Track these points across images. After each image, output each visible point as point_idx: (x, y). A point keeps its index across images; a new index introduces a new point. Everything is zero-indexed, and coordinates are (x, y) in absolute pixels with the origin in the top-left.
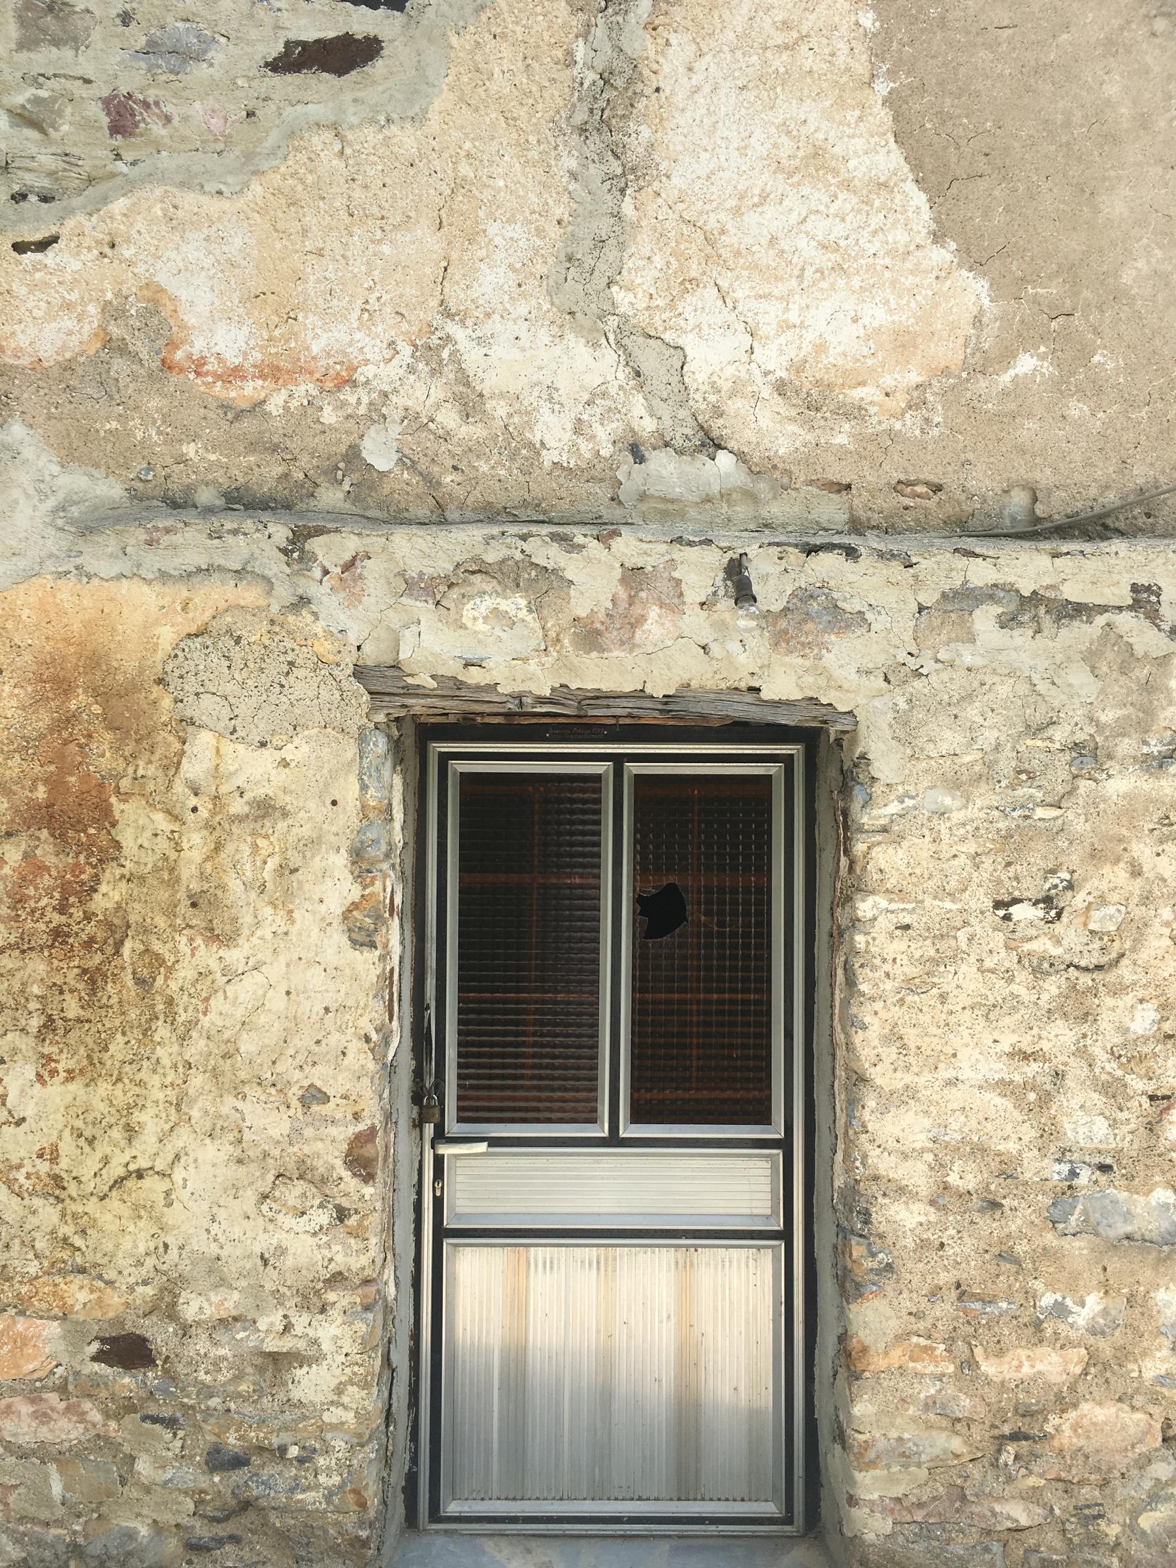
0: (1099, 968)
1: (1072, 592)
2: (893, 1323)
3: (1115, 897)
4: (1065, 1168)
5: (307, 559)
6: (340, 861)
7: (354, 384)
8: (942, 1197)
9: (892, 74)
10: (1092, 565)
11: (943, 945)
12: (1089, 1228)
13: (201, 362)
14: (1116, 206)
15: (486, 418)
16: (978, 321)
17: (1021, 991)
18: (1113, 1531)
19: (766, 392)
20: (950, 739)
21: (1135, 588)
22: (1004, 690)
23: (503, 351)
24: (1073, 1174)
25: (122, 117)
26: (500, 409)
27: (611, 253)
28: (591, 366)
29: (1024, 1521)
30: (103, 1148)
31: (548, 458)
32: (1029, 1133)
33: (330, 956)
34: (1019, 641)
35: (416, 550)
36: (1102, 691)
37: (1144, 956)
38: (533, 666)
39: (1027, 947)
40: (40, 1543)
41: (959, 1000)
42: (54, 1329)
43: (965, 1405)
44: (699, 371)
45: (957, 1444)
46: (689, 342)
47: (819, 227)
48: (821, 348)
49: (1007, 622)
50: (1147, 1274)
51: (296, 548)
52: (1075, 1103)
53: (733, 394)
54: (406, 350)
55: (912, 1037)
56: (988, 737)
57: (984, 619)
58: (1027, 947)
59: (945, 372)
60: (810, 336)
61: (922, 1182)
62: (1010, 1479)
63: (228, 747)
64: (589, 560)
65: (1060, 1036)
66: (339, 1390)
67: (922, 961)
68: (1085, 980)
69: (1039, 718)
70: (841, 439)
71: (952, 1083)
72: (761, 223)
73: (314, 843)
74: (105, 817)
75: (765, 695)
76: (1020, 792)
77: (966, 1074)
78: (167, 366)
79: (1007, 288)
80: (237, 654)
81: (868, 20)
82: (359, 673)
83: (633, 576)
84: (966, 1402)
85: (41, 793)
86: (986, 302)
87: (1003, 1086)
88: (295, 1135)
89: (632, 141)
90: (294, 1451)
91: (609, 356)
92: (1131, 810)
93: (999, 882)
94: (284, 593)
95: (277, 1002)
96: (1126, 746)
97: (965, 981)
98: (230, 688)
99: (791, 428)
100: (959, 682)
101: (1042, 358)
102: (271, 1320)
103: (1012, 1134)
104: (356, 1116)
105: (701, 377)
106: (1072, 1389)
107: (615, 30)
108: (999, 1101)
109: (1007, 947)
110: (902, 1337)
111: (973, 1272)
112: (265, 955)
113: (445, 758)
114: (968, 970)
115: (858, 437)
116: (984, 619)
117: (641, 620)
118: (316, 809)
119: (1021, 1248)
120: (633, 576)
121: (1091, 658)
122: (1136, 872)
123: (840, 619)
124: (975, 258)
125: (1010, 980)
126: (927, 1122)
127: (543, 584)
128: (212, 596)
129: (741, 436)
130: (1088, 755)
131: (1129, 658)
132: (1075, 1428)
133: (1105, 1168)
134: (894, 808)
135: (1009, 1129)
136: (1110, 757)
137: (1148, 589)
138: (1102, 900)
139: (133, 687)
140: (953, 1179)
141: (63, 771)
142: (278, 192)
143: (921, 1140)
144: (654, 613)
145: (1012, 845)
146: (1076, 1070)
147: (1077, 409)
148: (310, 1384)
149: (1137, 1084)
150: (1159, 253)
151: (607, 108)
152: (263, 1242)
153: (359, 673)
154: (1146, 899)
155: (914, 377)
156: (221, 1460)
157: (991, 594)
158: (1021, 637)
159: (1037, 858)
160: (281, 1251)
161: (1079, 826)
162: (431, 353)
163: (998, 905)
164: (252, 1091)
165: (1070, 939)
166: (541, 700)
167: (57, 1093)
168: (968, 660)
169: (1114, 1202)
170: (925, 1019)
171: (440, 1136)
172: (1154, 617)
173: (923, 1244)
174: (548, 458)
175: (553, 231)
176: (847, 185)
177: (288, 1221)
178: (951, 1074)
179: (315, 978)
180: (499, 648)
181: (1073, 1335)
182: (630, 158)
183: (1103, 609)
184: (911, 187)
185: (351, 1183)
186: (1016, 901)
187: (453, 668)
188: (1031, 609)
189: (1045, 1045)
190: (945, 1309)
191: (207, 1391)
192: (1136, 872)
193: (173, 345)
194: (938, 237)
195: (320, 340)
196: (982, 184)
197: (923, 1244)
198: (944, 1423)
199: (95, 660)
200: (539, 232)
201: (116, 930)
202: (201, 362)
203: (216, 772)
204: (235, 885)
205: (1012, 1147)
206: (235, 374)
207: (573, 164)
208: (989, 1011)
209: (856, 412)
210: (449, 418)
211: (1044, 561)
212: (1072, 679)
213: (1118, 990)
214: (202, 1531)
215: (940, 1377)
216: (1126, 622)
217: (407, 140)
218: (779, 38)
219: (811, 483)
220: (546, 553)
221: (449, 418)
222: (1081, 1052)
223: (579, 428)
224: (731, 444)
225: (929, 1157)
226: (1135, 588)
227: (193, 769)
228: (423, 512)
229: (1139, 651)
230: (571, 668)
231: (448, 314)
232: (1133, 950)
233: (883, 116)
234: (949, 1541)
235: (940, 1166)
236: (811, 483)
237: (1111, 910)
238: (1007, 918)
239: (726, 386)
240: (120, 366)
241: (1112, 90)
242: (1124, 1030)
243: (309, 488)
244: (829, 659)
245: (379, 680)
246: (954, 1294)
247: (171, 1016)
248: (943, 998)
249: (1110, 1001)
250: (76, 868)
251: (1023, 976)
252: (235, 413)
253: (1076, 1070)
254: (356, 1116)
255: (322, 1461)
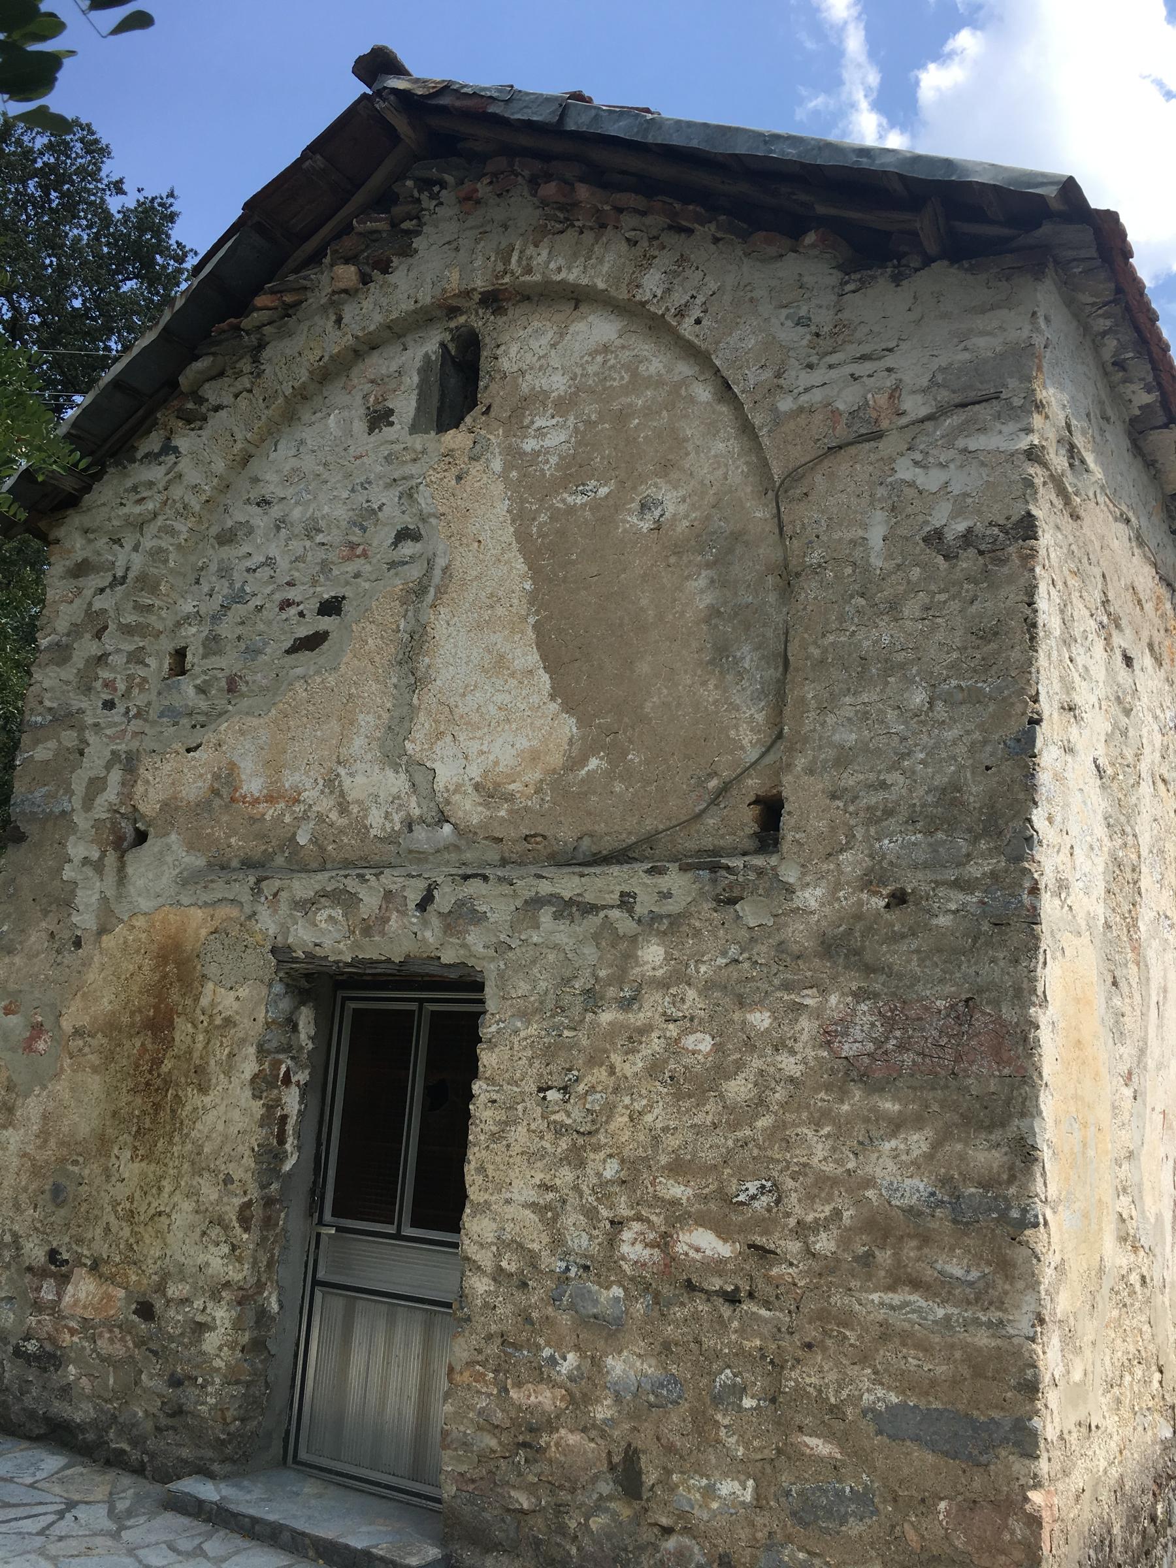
0: (590, 1133)
1: (589, 898)
2: (466, 1354)
3: (599, 1088)
4: (563, 1265)
5: (260, 891)
6: (252, 1050)
7: (298, 801)
8: (499, 1276)
9: (537, 612)
10: (599, 883)
11: (510, 1113)
12: (572, 1306)
13: (245, 797)
14: (643, 668)
15: (349, 813)
16: (571, 742)
17: (548, 1146)
18: (573, 1524)
19: (470, 790)
20: (523, 987)
21: (622, 894)
22: (551, 957)
23: (360, 779)
24: (567, 1269)
25: (232, 686)
26: (355, 809)
27: (406, 724)
28: (396, 782)
29: (525, 1506)
30: (150, 1198)
31: (373, 832)
32: (546, 1239)
33: (243, 1103)
34: (562, 927)
35: (302, 887)
36: (600, 958)
37: (612, 1127)
38: (341, 945)
39: (553, 1117)
40: (102, 1410)
41: (516, 1149)
42: (121, 1293)
43: (499, 1417)
44: (441, 783)
45: (493, 1443)
46: (437, 766)
47: (500, 698)
48: (496, 763)
49: (557, 916)
50: (601, 1344)
51: (256, 890)
52: (570, 1221)
53: (455, 791)
54: (321, 782)
55: (490, 1169)
56: (543, 985)
57: (546, 916)
58: (553, 1117)
59: (554, 771)
60: (492, 757)
61: (489, 1264)
62: (520, 1475)
63: (218, 990)
64: (370, 888)
65: (565, 1176)
66: (220, 1349)
67: (500, 1123)
68: (580, 1141)
69: (568, 974)
70: (502, 813)
71: (508, 1202)
72: (473, 700)
73: (243, 1041)
74: (171, 1026)
75: (443, 960)
76: (557, 1019)
77: (516, 1196)
78: (233, 800)
79: (583, 722)
80: (226, 942)
81: (528, 585)
82: (273, 951)
83: (388, 895)
84: (499, 1415)
85: (151, 1013)
86: (574, 730)
87: (533, 1206)
88: (219, 1201)
89: (420, 665)
90: (200, 1380)
91: (403, 776)
92: (615, 1029)
93: (541, 1075)
94: (248, 910)
95: (220, 1127)
96: (611, 992)
97: (519, 1135)
98: (223, 960)
99: (480, 809)
100: (531, 953)
101: (602, 759)
102: (198, 1304)
103: (537, 1241)
104: (245, 1193)
105: (441, 785)
106: (558, 1417)
107: (417, 611)
108: (532, 1216)
109: (543, 1117)
110: (470, 1364)
111: (509, 1326)
112: (218, 1101)
113: (344, 999)
114: (522, 1129)
115: (510, 812)
116: (546, 916)
117: (389, 919)
118: (246, 1023)
119: (535, 1315)
120: (388, 895)
121: (596, 937)
122: (612, 1071)
123: (478, 918)
124: (568, 708)
125: (542, 1138)
126: (494, 1226)
127: (346, 900)
128: (225, 911)
129: (458, 815)
130: (592, 999)
131: (617, 938)
132: (557, 1445)
133: (586, 1268)
134: (494, 1028)
135: (535, 1236)
136: (602, 999)
137: (628, 895)
138: (592, 1090)
139: (189, 960)
140: (504, 1264)
141: (160, 1002)
142: (281, 712)
143: (490, 1237)
144: (394, 915)
145: (549, 1053)
146: (573, 1199)
147: (618, 787)
148: (211, 1341)
149: (604, 1213)
150: (665, 691)
151: (412, 650)
152: (201, 1259)
153: (273, 951)
154: (616, 1090)
155: (538, 776)
156: (176, 1382)
157: (552, 899)
158: (563, 926)
159: (561, 1062)
160: (207, 1264)
161: (585, 1042)
162: (331, 783)
163: (541, 1090)
164: (206, 1174)
165: (575, 1115)
166: (347, 965)
167: (137, 1166)
168: (535, 939)
169: (590, 1292)
170: (498, 1159)
171: (321, 1223)
172: (631, 911)
173: (486, 1305)
174: (373, 832)
175: (386, 716)
176: (512, 675)
177: (212, 1249)
178: (508, 1195)
179: (236, 1114)
180: (327, 936)
181: (559, 1379)
182: (419, 674)
183: (604, 907)
184: (541, 671)
185: (238, 1230)
186: (550, 1088)
187: (310, 947)
188: (570, 908)
189: (558, 1182)
190: (493, 1349)
191: (171, 1338)
192: (612, 1071)
193: (236, 790)
194: (553, 697)
195: (290, 780)
196: (577, 664)
197: (486, 1305)
198: (489, 1427)
199: (178, 947)
200: (379, 717)
201: (167, 1083)
202: (245, 797)
203: (213, 1004)
204: (212, 1062)
205: (535, 1246)
206: (256, 801)
207: (394, 680)
208: (532, 1156)
209: (509, 798)
210: (334, 816)
211: (576, 879)
212: (586, 951)
213: (597, 1148)
214: (164, 1421)
215: (489, 1395)
216: (615, 914)
217: (331, 680)
218: (488, 602)
219: (486, 838)
220: (352, 885)
221: (334, 816)
222: (576, 1188)
223: (387, 815)
224: (452, 820)
225: (494, 1248)
226: (622, 894)
227: (204, 1002)
228: (315, 865)
229: (621, 932)
230: (360, 947)
231: (339, 763)
232: (607, 1122)
233: (531, 634)
234: (484, 1509)
235: (498, 1256)
236: (486, 838)
237: (598, 1096)
238: (544, 1098)
239: (451, 788)
240: (217, 802)
241: (644, 602)
242: (599, 1175)
243: (270, 857)
244: (470, 939)
245: (282, 953)
246: (499, 1341)
247: (181, 1129)
248: (508, 1146)
249: (592, 1156)
250: (158, 1051)
251: (549, 1136)
252: (253, 820)
253: (573, 1199)
254: (245, 1193)
255: (209, 1389)
